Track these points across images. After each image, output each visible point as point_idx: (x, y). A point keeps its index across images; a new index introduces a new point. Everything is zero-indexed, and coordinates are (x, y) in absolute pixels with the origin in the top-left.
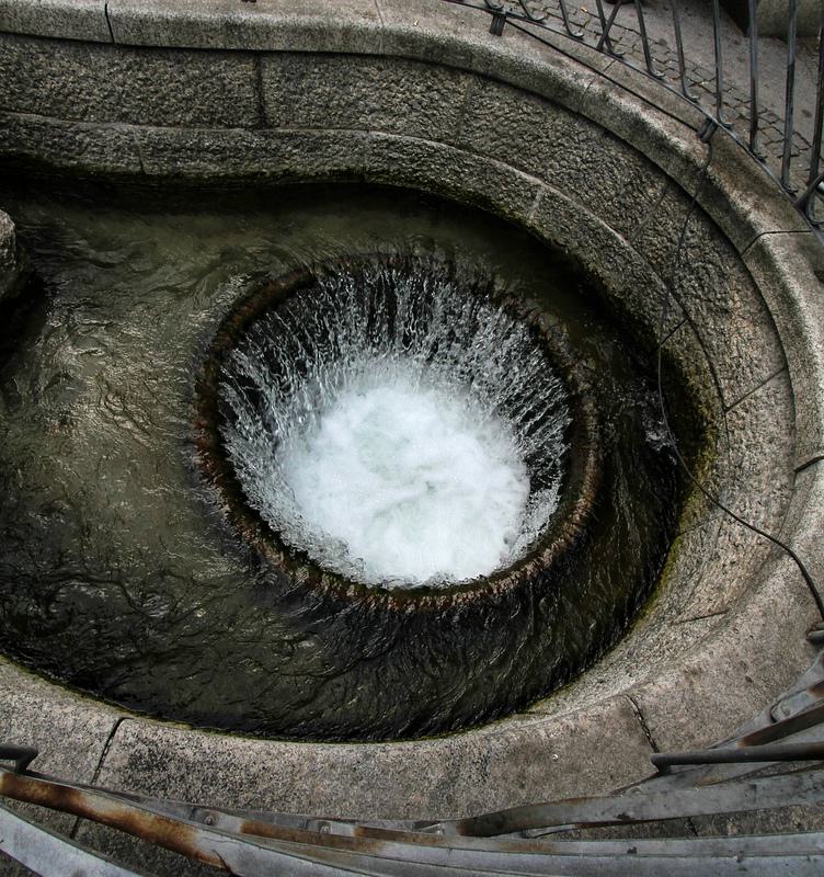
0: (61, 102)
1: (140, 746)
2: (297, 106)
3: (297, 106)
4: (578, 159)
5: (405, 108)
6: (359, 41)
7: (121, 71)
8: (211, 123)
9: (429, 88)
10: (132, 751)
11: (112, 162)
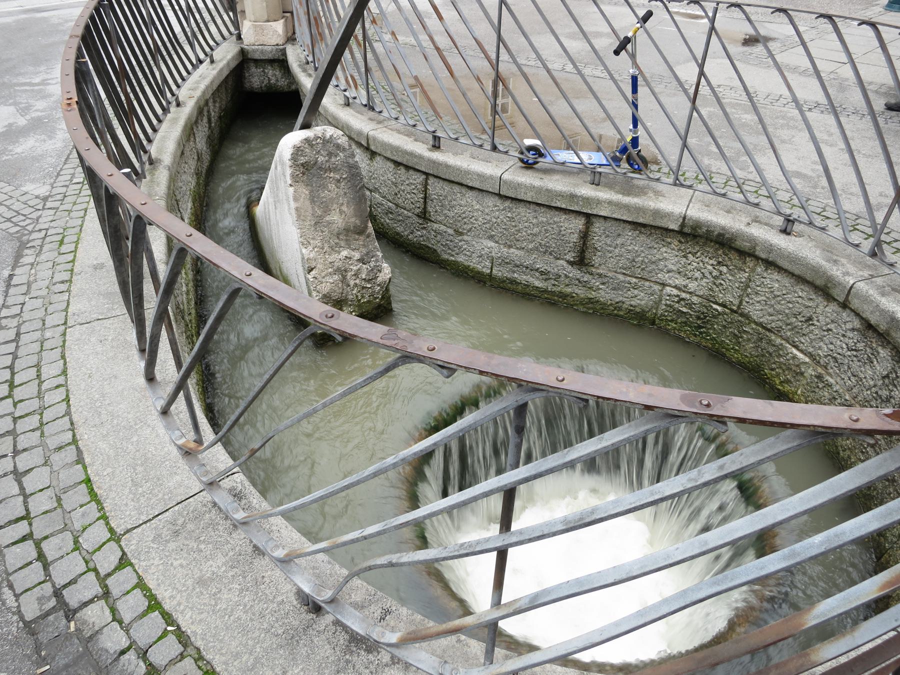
0: (459, 221)
1: (239, 485)
2: (610, 255)
3: (610, 255)
4: (844, 346)
5: (698, 274)
6: (665, 220)
7: (498, 210)
8: (545, 253)
9: (719, 263)
10: (235, 485)
11: (474, 263)
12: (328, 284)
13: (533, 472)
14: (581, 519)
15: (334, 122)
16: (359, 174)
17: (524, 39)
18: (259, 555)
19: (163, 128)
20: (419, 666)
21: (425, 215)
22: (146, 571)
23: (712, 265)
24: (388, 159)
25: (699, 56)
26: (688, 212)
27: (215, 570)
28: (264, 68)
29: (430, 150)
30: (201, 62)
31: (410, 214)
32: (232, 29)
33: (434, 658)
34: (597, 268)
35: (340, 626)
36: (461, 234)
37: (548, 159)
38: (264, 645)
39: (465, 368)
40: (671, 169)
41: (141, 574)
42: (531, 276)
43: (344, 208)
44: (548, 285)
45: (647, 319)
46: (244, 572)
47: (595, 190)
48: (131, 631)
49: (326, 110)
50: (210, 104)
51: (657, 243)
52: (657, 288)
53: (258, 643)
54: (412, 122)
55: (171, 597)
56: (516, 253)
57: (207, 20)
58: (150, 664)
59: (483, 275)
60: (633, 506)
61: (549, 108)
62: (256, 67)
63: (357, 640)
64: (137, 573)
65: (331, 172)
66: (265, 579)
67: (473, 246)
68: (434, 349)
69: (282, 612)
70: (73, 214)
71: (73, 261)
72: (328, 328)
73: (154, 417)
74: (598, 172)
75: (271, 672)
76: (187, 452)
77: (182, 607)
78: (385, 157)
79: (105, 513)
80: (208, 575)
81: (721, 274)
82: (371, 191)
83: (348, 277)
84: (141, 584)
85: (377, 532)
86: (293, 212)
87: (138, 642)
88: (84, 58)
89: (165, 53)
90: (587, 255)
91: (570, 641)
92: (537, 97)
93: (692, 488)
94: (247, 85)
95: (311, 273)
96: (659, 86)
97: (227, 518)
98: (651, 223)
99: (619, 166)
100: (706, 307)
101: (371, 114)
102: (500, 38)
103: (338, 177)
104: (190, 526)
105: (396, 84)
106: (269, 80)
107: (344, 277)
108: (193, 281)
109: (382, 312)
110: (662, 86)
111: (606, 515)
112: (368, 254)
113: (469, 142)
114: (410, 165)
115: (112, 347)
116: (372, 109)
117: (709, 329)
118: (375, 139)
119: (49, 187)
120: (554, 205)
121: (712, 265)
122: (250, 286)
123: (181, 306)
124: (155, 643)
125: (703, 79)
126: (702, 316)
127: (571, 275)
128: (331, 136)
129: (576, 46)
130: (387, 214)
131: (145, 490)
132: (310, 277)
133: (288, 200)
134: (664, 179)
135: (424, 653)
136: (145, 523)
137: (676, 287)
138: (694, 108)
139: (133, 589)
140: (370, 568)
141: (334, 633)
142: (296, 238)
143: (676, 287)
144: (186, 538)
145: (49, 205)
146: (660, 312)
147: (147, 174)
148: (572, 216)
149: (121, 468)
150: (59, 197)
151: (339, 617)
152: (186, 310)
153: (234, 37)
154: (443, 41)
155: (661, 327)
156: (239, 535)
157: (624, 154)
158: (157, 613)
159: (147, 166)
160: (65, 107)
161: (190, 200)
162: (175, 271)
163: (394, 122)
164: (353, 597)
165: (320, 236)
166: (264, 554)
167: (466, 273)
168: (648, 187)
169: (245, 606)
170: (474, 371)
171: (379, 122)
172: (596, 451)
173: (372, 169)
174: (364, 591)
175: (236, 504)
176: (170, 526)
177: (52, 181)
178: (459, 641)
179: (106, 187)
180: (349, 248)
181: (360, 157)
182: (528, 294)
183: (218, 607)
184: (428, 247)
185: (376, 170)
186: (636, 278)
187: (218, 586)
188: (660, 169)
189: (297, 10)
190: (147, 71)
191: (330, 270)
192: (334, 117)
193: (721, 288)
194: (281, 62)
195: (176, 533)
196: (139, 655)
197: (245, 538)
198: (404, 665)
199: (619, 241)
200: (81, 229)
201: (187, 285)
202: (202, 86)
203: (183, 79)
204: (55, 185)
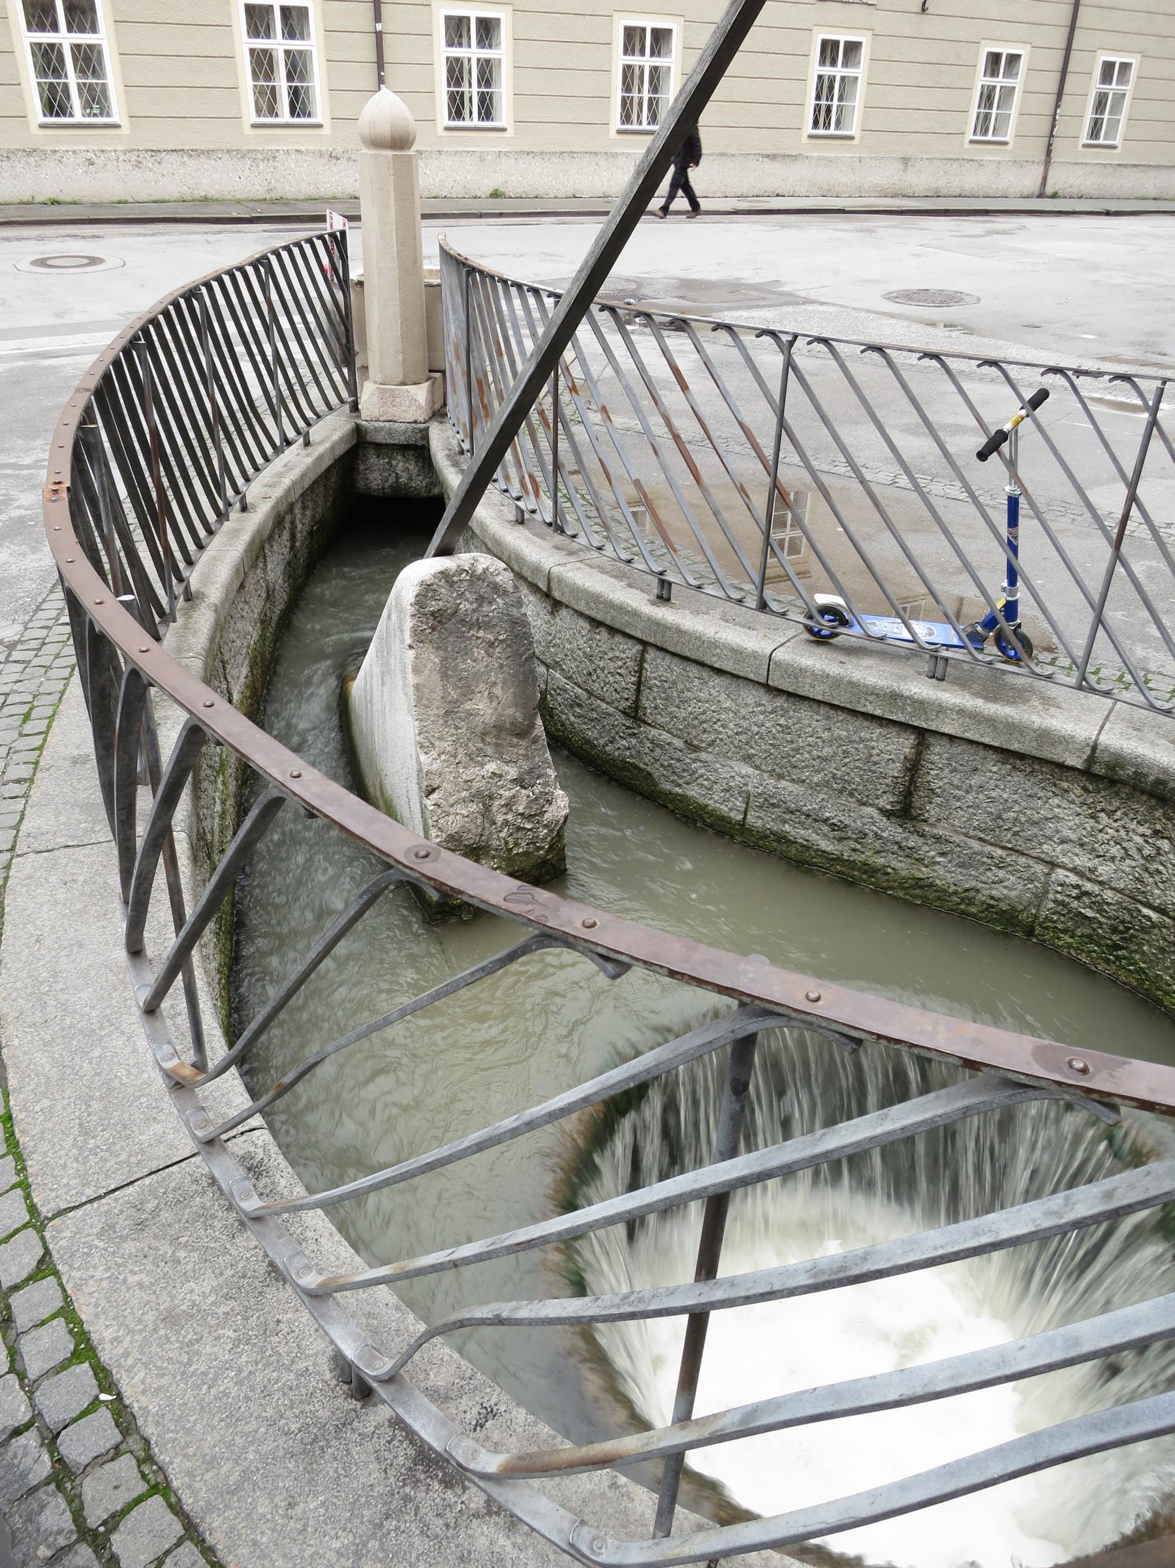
0: (694, 727)
1: (260, 1151)
2: (958, 804)
3: (958, 804)
5: (1115, 850)
6: (1060, 749)
7: (763, 713)
8: (841, 792)
9: (1156, 833)
10: (252, 1149)
12: (458, 817)
13: (757, 1168)
14: (843, 1268)
15: (495, 549)
16: (527, 636)
17: (826, 431)
18: (277, 1280)
19: (215, 545)
20: (534, 1524)
21: (637, 712)
22: (78, 1287)
23: (1143, 835)
24: (581, 614)
25: (1130, 473)
26: (1102, 738)
27: (198, 1299)
28: (391, 458)
29: (653, 603)
30: (289, 443)
31: (611, 710)
32: (344, 394)
33: (562, 1512)
34: (932, 825)
35: (401, 1429)
36: (697, 749)
37: (856, 630)
38: (264, 1449)
39: (645, 962)
40: (1074, 662)
41: (69, 1292)
42: (815, 831)
43: (498, 691)
44: (843, 850)
45: (1019, 924)
46: (246, 1308)
47: (936, 688)
48: (38, 1394)
49: (483, 527)
50: (297, 511)
51: (1043, 788)
52: (1040, 868)
53: (252, 1443)
54: (625, 556)
55: (115, 1339)
56: (790, 789)
57: (305, 380)
58: (60, 1461)
59: (730, 822)
60: (940, 1252)
61: (864, 546)
62: (378, 456)
63: (430, 1460)
64: (64, 1290)
65: (479, 628)
66: (282, 1326)
67: (716, 770)
68: (594, 925)
69: (303, 1391)
70: (52, 673)
71: (40, 748)
72: (417, 875)
73: (134, 1019)
74: (942, 658)
75: (267, 1501)
76: (177, 1083)
77: (130, 1361)
78: (576, 611)
79: (26, 1178)
80: (183, 1307)
81: (1159, 854)
82: (548, 666)
83: (495, 809)
84: (67, 1311)
85: (476, 1255)
86: (411, 690)
87: (46, 1416)
88: (94, 422)
89: (231, 428)
90: (917, 801)
91: (815, 1509)
92: (843, 526)
93: (1050, 1228)
94: (361, 484)
95: (431, 797)
96: (1060, 519)
97: (230, 1208)
98: (1034, 753)
99: (981, 650)
100: (1129, 910)
101: (559, 539)
102: (782, 424)
103: (491, 637)
104: (166, 1216)
105: (605, 493)
106: (398, 477)
107: (488, 808)
108: (235, 797)
109: (547, 873)
110: (1067, 520)
111: (889, 1265)
112: (530, 771)
113: (721, 594)
114: (617, 626)
115: (83, 894)
116: (561, 530)
117: (1133, 951)
118: (560, 580)
119: (20, 628)
120: (861, 710)
121: (1143, 835)
122: (295, 794)
123: (209, 836)
124: (75, 1420)
125: (1134, 510)
126: (1121, 928)
127: (885, 835)
128: (485, 570)
129: (916, 446)
130: (572, 706)
131: (99, 1143)
132: (429, 803)
133: (403, 671)
134: (1061, 677)
135: (545, 1500)
136: (91, 1201)
137: (1074, 870)
138: (1117, 556)
139: (54, 1317)
140: (462, 1324)
141: (389, 1442)
142: (412, 735)
143: (1074, 870)
144: (156, 1237)
145: (16, 655)
146: (1044, 913)
147: (178, 615)
148: (893, 731)
149: (65, 1102)
150: (34, 644)
151: (400, 1411)
152: (216, 843)
153: (347, 407)
154: (688, 428)
155: (1044, 941)
156: (247, 1240)
157: (991, 630)
158: (87, 1364)
159: (181, 602)
160: (49, 495)
161: (246, 662)
162: (183, 764)
163: (595, 554)
164: (432, 1377)
165: (453, 735)
166: (285, 1281)
167: (701, 817)
168: (1032, 690)
169: (240, 1371)
170: (660, 971)
171: (571, 553)
172: (872, 1139)
173: (553, 630)
174: (453, 1369)
175: (248, 1184)
176: (132, 1211)
177: (27, 618)
178: (614, 1486)
179: (91, 621)
180: (501, 758)
181: (533, 610)
182: (807, 863)
183: (192, 1369)
184: (637, 767)
185: (560, 632)
186: (1003, 848)
187: (198, 1329)
188: (1055, 659)
189: (451, 368)
190: (199, 454)
191: (464, 794)
192: (496, 540)
193: (1157, 878)
194: (419, 450)
195: (141, 1225)
196: (43, 1439)
197: (256, 1247)
198: (508, 1519)
199: (975, 781)
200: (60, 698)
201: (223, 803)
202: (287, 482)
203: (257, 469)
204: (30, 625)
